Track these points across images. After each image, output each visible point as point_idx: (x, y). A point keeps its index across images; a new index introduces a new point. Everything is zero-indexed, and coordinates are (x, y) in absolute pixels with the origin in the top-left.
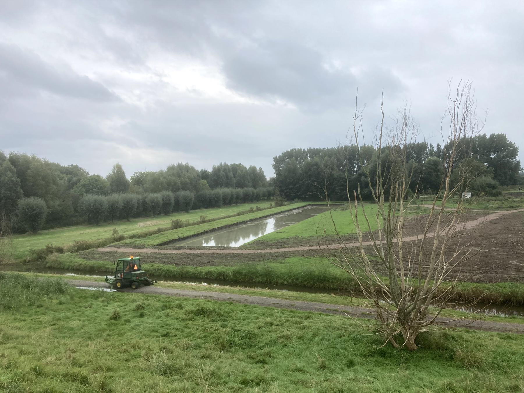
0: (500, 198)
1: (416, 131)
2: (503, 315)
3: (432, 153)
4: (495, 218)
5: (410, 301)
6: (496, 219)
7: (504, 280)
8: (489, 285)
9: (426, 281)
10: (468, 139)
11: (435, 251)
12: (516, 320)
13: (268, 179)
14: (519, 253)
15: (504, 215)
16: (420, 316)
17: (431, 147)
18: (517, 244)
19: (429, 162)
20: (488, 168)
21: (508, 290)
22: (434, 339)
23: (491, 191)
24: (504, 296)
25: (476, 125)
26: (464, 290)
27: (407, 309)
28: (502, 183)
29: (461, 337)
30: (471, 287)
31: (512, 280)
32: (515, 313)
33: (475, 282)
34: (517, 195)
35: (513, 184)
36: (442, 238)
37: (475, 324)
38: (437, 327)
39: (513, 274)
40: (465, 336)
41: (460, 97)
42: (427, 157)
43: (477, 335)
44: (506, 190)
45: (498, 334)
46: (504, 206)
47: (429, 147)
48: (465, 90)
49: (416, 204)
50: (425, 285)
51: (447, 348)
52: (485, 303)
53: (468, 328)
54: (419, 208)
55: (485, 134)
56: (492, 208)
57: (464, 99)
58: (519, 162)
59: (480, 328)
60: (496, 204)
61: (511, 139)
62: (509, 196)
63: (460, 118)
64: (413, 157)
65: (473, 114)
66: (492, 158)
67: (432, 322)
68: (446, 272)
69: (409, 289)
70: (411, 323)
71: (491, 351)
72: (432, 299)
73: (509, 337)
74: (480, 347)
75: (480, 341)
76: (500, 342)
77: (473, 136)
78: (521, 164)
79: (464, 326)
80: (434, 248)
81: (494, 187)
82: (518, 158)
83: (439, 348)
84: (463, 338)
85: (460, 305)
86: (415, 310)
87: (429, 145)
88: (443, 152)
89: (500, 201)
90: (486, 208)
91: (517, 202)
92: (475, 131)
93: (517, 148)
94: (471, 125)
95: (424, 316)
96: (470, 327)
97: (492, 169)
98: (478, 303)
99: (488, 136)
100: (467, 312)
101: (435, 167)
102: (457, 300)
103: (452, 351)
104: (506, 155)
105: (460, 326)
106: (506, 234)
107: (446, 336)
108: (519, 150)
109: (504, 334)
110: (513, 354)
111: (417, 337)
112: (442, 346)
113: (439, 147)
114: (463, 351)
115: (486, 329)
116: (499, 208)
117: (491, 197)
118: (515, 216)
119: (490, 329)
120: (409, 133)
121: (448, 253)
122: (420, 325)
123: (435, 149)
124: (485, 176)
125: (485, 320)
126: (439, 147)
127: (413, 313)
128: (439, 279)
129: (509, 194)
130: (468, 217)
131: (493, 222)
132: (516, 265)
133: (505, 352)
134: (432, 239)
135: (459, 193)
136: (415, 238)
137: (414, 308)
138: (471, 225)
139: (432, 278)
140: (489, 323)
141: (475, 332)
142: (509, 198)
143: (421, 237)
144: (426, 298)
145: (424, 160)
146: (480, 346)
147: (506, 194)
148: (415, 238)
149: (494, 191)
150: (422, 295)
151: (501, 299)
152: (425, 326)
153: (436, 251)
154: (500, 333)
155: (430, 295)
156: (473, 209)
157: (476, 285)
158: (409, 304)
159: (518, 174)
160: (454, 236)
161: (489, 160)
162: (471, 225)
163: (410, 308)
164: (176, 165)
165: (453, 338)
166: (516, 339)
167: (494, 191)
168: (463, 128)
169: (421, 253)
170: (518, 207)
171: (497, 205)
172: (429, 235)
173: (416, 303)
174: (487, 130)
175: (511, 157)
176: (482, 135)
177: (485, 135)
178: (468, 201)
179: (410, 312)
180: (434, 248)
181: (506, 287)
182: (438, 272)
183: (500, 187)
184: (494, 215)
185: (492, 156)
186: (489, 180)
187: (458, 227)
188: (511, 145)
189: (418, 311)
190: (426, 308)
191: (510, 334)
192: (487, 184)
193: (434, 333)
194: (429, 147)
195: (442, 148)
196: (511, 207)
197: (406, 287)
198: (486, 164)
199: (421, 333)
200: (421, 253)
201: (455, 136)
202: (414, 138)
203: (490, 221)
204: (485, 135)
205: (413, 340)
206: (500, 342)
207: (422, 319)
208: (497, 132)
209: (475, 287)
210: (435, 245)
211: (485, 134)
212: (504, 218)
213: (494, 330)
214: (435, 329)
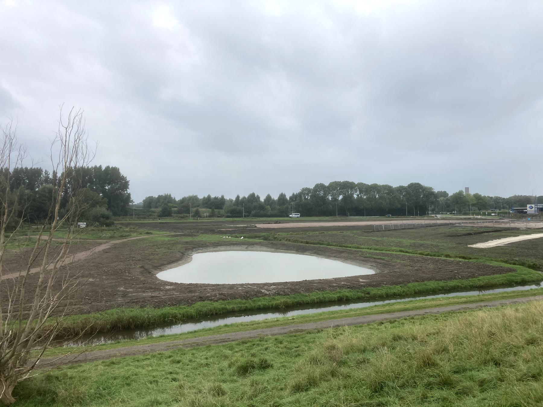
0: (112, 228)
1: (22, 153)
2: (109, 342)
3: (47, 180)
4: (107, 247)
5: (8, 347)
6: (109, 248)
7: (111, 307)
8: (98, 315)
9: (29, 322)
10: (84, 168)
11: (40, 286)
12: (120, 344)
13: (288, 199)
14: (126, 279)
15: (115, 244)
16: (19, 362)
17: (46, 174)
18: (125, 272)
19: (44, 190)
20: (103, 198)
21: (115, 316)
22: (35, 385)
23: (103, 222)
24: (111, 323)
25: (87, 155)
26: (74, 323)
27: (3, 358)
28: (115, 214)
29: (65, 375)
30: (80, 319)
31: (119, 306)
32: (120, 337)
33: (85, 313)
34: (127, 225)
35: (124, 215)
36: (48, 272)
37: (81, 358)
38: (40, 371)
39: (120, 300)
40: (70, 373)
41: (71, 125)
42: (42, 184)
43: (81, 369)
44: (119, 221)
45: (103, 362)
46: (116, 235)
47: (44, 173)
48: (77, 118)
49: (26, 235)
50: (27, 326)
51: (50, 391)
52: (92, 333)
53: (75, 363)
54: (30, 239)
55: (101, 166)
56: (105, 238)
57: (75, 126)
58: (129, 194)
59: (85, 361)
60: (109, 234)
61: (123, 172)
62: (120, 226)
63: (71, 145)
64: (24, 183)
65: (85, 143)
66: (106, 189)
67: (33, 367)
68: (52, 308)
69: (8, 332)
70: (9, 373)
71: (95, 382)
72: (35, 340)
73: (113, 363)
74: (83, 380)
75: (85, 374)
76: (103, 370)
77: (90, 167)
78: (131, 196)
79: (69, 362)
80: (39, 283)
81: (107, 218)
82: (129, 191)
83: (40, 394)
84: (67, 375)
85: (68, 340)
86: (13, 357)
87: (44, 171)
88: (60, 180)
89: (112, 230)
90: (100, 238)
91: (127, 231)
92: (86, 161)
93: (128, 182)
94: (83, 154)
95: (24, 362)
96: (76, 362)
97: (106, 200)
98: (54, 339)
99: (103, 168)
100: (75, 346)
101: (49, 195)
102: (64, 336)
103: (55, 393)
104: (119, 187)
105: (66, 364)
106: (116, 262)
107: (49, 378)
108: (130, 183)
109: (108, 361)
110: (115, 379)
111: (15, 389)
112: (43, 391)
113: (55, 174)
114: (66, 390)
115: (92, 360)
116: (112, 238)
117: (104, 227)
118: (124, 245)
119: (96, 359)
120: (14, 155)
121: (57, 287)
122: (20, 373)
123: (51, 176)
124: (100, 206)
125: (92, 350)
126: (55, 174)
127: (10, 361)
128: (44, 316)
129: (122, 224)
130: (82, 247)
131: (105, 251)
132: (123, 291)
133: (108, 379)
134: (38, 274)
135: (68, 223)
136: (16, 275)
137: (13, 355)
138: (81, 256)
139: (36, 316)
140: (97, 353)
141: (81, 366)
142: (121, 228)
143: (24, 273)
144: (27, 341)
145: (38, 187)
146: (84, 379)
147: (118, 224)
148: (16, 275)
149: (108, 221)
150: (23, 339)
151: (108, 326)
152: (25, 373)
153: (41, 285)
154: (105, 360)
155: (32, 337)
156: (87, 239)
157: (85, 316)
158: (7, 351)
159: (129, 205)
160: (63, 268)
161: (104, 191)
162: (81, 256)
163: (8, 356)
164: (11, 170)
165: (57, 378)
166: (119, 363)
167: (108, 221)
168: (75, 156)
169: (23, 292)
170: (127, 236)
171: (110, 235)
172: (33, 271)
173: (15, 347)
174: (103, 161)
175: (123, 190)
176: (98, 166)
177: (100, 167)
178: (82, 231)
179: (8, 360)
180: (39, 283)
181: (113, 314)
182: (43, 309)
183: (113, 217)
184: (107, 244)
185: (107, 188)
186: (103, 210)
187: (67, 261)
188: (123, 178)
189: (17, 358)
190: (28, 352)
191: (114, 359)
192: (102, 214)
193: (35, 379)
194: (44, 173)
195: (59, 175)
196: (122, 237)
197: (4, 331)
198: (101, 195)
199: (20, 383)
200: (23, 292)
201: (66, 163)
202: (20, 161)
203: (103, 250)
204: (100, 167)
205: (10, 393)
206: (103, 370)
207: (22, 365)
208: (112, 164)
209: (85, 319)
210: (40, 280)
211: (101, 166)
212: (115, 247)
213: (100, 359)
214: (37, 374)
